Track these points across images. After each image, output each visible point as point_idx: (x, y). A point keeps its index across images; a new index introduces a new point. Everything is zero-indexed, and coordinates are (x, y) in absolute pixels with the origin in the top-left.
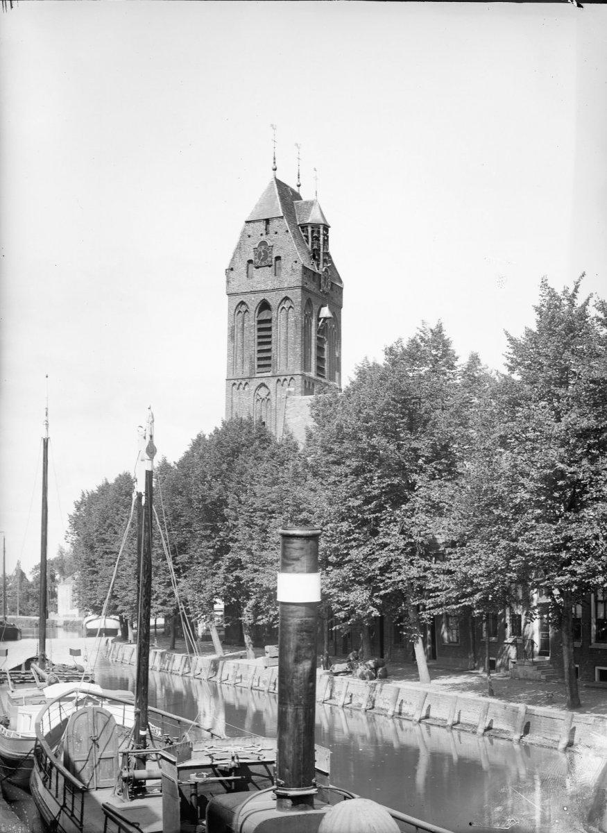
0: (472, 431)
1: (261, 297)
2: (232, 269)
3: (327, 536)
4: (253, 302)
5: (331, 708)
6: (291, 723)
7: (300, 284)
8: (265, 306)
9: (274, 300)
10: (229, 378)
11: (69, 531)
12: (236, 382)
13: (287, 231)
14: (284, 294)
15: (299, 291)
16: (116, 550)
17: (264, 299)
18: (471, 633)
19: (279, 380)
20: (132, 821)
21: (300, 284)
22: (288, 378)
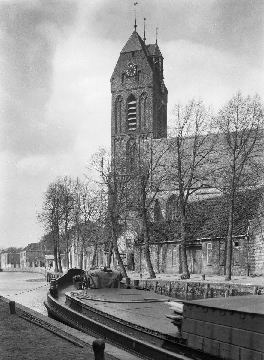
0: (238, 288)
1: (130, 93)
2: (114, 78)
3: (123, 116)
4: (125, 96)
5: (188, 335)
6: (73, 341)
7: (152, 85)
8: (132, 98)
9: (137, 94)
10: (113, 135)
11: (190, 308)
12: (116, 137)
13: (144, 57)
14: (143, 91)
15: (151, 89)
16: (239, 349)
17: (132, 94)
18: (215, 324)
19: (141, 136)
20: (21, 318)
21: (152, 85)
22: (146, 134)
